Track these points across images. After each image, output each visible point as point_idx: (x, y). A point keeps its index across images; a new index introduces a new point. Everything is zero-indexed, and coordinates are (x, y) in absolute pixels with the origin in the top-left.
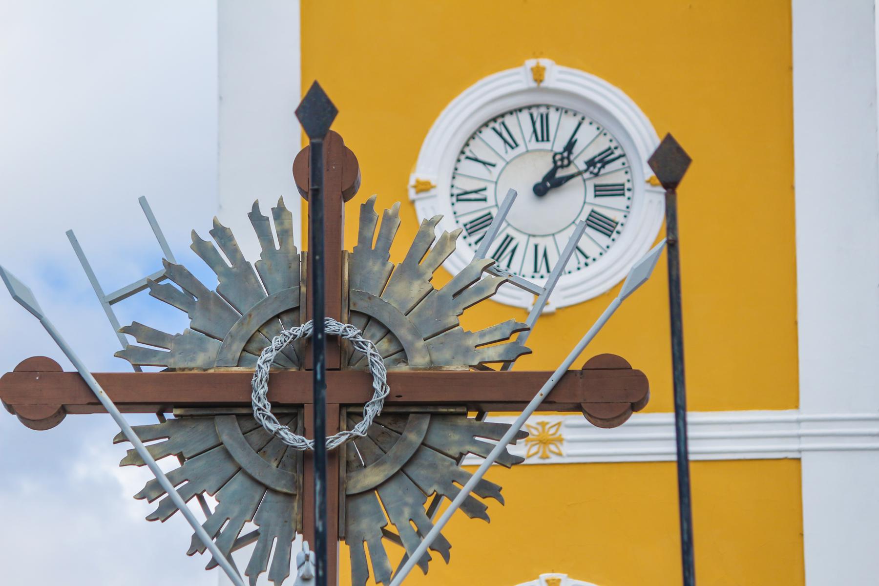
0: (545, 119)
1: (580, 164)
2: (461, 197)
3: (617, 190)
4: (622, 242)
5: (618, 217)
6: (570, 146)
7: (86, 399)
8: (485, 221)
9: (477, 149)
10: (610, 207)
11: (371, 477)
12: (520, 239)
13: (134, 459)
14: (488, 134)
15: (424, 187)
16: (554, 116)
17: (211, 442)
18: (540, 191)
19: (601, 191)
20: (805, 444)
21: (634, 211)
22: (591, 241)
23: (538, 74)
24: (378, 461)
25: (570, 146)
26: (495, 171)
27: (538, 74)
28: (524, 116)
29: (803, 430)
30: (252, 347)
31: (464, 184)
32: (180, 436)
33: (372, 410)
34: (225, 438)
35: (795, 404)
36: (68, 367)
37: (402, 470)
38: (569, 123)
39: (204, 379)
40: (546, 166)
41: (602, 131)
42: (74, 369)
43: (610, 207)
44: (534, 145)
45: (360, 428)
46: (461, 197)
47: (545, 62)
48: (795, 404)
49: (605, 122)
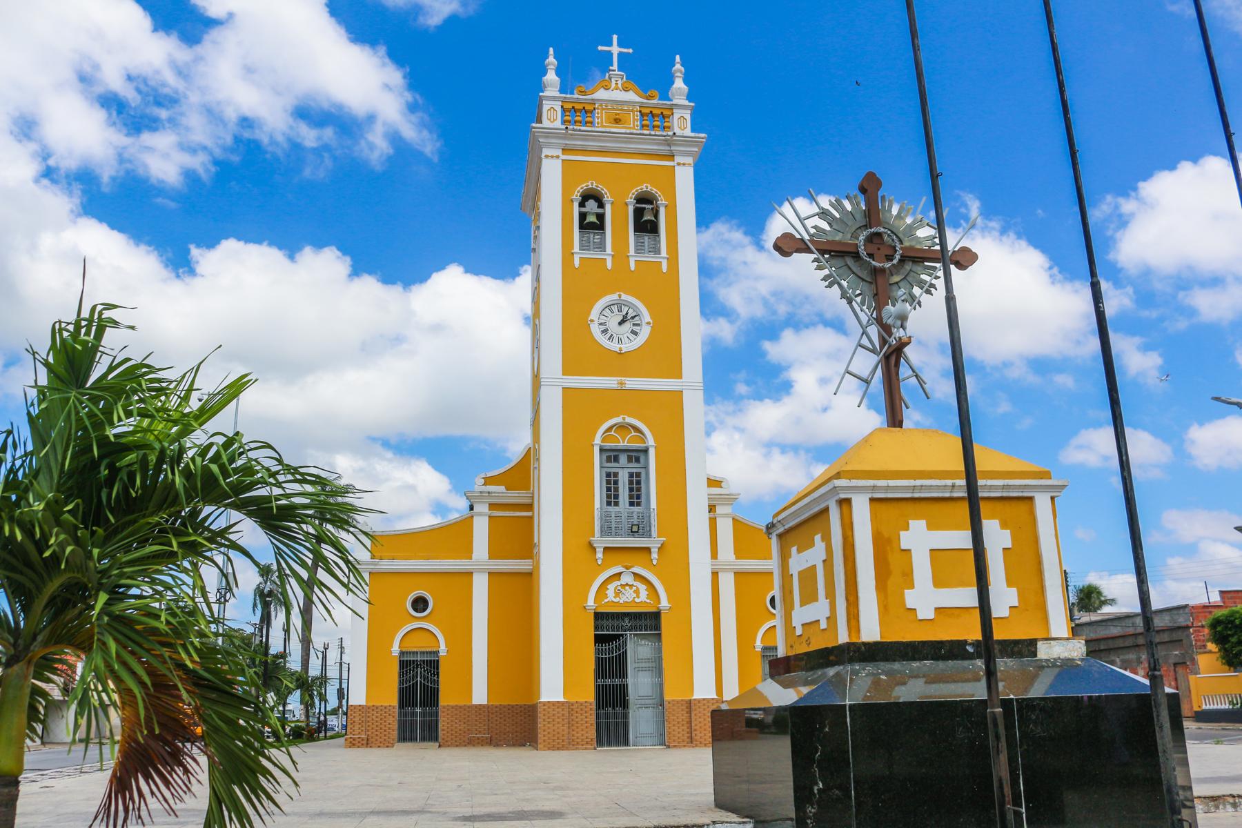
0: (621, 307)
1: (629, 318)
2: (600, 324)
3: (638, 325)
4: (639, 338)
5: (638, 331)
6: (627, 314)
7: (804, 247)
8: (607, 330)
9: (604, 313)
10: (636, 329)
11: (896, 279)
12: (615, 335)
13: (819, 268)
14: (607, 309)
15: (592, 321)
16: (623, 306)
17: (843, 264)
18: (620, 324)
19: (634, 325)
20: (684, 388)
21: (642, 330)
22: (632, 337)
23: (620, 296)
24: (897, 273)
25: (627, 314)
26: (609, 319)
27: (620, 296)
28: (616, 306)
29: (684, 384)
30: (855, 236)
31: (601, 321)
32: (833, 261)
33: (898, 257)
34: (849, 263)
35: (681, 378)
36: (798, 236)
37: (905, 278)
38: (626, 309)
39: (839, 243)
40: (621, 318)
41: (634, 311)
42: (799, 237)
43: (636, 329)
44: (618, 313)
45: (895, 262)
46: (600, 324)
47: (621, 293)
48: (681, 378)
49: (635, 309)
